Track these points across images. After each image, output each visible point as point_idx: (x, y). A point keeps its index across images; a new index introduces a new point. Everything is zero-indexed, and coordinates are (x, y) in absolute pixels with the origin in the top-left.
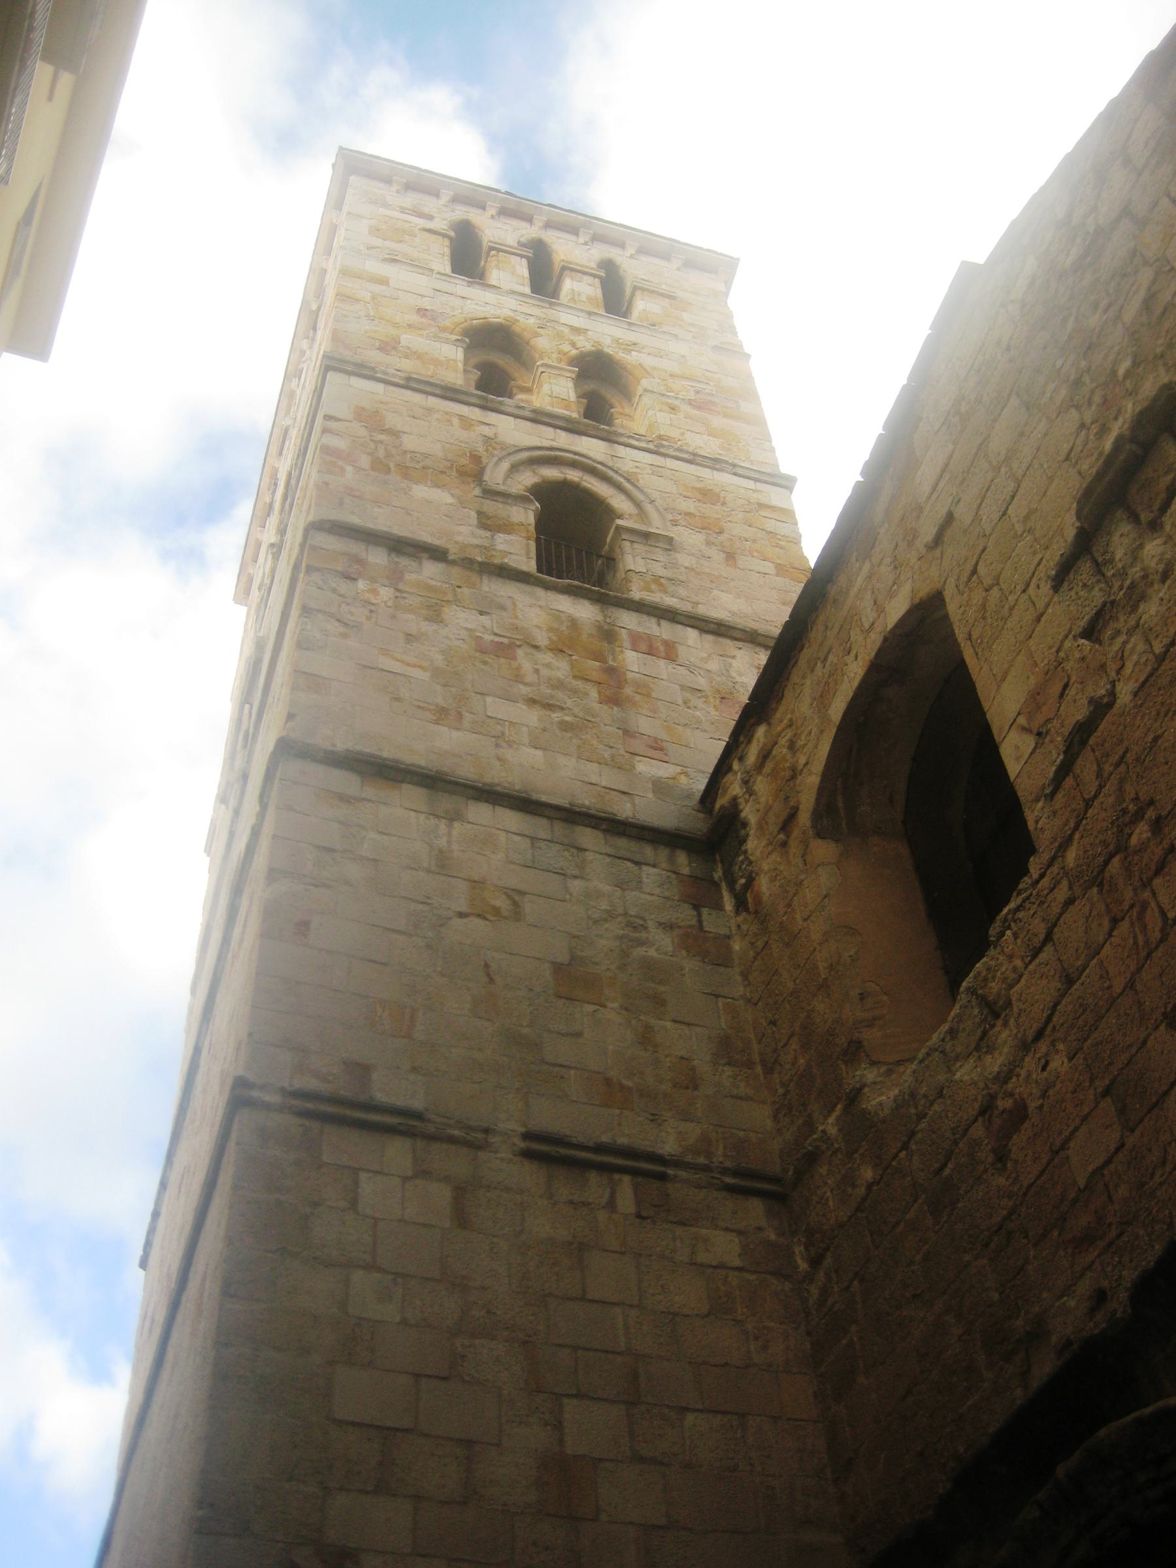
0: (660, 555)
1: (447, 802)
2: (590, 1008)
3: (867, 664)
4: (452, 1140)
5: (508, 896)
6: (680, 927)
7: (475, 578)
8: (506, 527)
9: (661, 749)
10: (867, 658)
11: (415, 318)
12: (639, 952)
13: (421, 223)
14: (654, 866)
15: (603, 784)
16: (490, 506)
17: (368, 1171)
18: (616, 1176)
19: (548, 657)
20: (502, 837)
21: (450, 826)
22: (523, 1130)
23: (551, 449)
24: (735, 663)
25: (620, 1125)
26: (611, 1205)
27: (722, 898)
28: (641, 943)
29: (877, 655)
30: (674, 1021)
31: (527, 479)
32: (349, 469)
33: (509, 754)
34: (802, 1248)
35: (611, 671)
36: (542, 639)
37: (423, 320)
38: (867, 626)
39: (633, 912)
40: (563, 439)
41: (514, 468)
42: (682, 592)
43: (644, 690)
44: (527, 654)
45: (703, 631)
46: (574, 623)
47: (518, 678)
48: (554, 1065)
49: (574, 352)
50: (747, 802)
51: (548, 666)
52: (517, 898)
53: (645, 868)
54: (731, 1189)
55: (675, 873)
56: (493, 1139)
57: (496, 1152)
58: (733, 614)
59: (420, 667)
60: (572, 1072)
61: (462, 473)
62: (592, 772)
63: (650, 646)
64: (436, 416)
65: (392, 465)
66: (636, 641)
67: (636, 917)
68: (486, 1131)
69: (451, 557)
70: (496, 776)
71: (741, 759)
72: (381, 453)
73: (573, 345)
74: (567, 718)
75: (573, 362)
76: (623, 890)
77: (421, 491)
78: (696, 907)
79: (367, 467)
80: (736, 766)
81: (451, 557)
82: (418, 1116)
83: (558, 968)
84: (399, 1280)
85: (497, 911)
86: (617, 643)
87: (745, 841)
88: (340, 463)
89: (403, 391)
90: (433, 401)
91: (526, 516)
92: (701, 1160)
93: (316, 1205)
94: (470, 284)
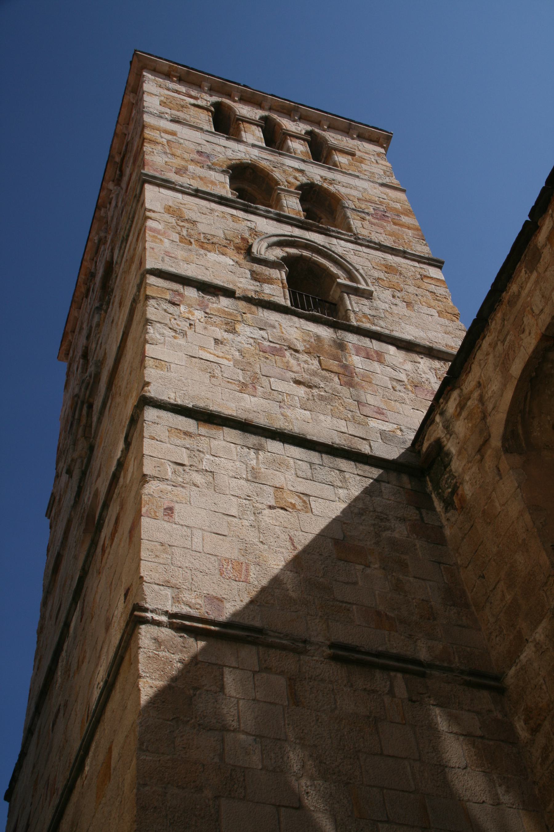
0: (365, 302)
1: (253, 440)
2: (362, 567)
3: (539, 337)
4: (283, 648)
5: (299, 497)
6: (410, 520)
7: (254, 308)
8: (269, 281)
9: (383, 414)
10: (539, 332)
11: (196, 157)
12: (387, 534)
13: (192, 101)
14: (388, 483)
15: (350, 433)
16: (257, 267)
17: (230, 667)
18: (392, 674)
19: (305, 357)
20: (291, 461)
21: (257, 454)
22: (328, 643)
23: (291, 236)
24: (421, 366)
25: (389, 641)
26: (391, 692)
27: (432, 502)
28: (386, 529)
29: (547, 328)
30: (415, 577)
31: (277, 253)
32: (166, 240)
33: (289, 412)
34: (522, 723)
35: (345, 367)
36: (300, 346)
37: (200, 158)
38: (537, 312)
39: (379, 509)
40: (297, 232)
41: (270, 246)
42: (382, 323)
43: (367, 379)
44: (291, 354)
45: (399, 348)
46: (318, 338)
47: (288, 368)
48: (342, 602)
49: (298, 183)
50: (448, 440)
51: (306, 362)
52: (305, 498)
53: (383, 484)
54: (468, 684)
55: (401, 487)
56: (308, 647)
57: (312, 656)
58: (416, 338)
59: (226, 358)
60: (354, 607)
61: (238, 249)
62: (342, 425)
63: (368, 354)
64: (216, 214)
65: (192, 240)
66: (358, 350)
67: (381, 512)
68: (305, 642)
69: (237, 295)
70: (279, 424)
71: (442, 414)
72: (184, 233)
73: (296, 178)
74: (322, 393)
75: (299, 188)
76: (371, 496)
77: (213, 257)
78: (418, 508)
79: (178, 241)
80: (438, 419)
81: (237, 295)
82: (260, 631)
83: (336, 542)
84: (258, 739)
85: (293, 506)
86: (347, 351)
87: (449, 464)
88: (159, 237)
89: (193, 198)
90: (213, 205)
91: (280, 275)
92: (446, 664)
93: (196, 689)
94: (228, 139)
